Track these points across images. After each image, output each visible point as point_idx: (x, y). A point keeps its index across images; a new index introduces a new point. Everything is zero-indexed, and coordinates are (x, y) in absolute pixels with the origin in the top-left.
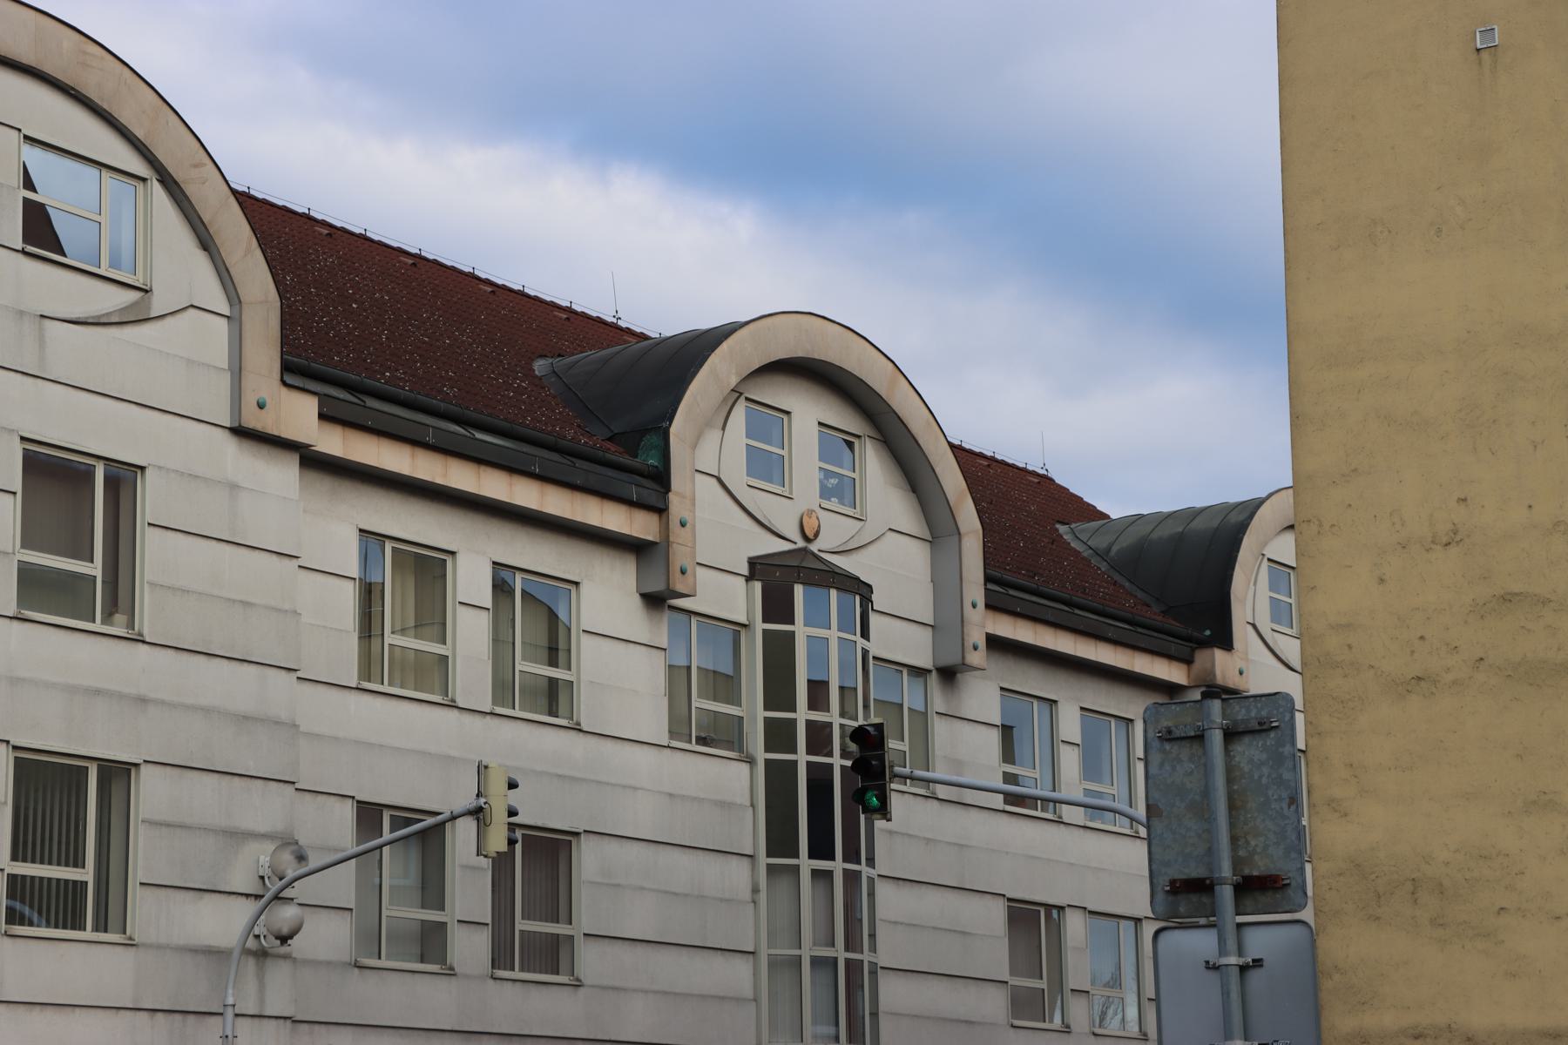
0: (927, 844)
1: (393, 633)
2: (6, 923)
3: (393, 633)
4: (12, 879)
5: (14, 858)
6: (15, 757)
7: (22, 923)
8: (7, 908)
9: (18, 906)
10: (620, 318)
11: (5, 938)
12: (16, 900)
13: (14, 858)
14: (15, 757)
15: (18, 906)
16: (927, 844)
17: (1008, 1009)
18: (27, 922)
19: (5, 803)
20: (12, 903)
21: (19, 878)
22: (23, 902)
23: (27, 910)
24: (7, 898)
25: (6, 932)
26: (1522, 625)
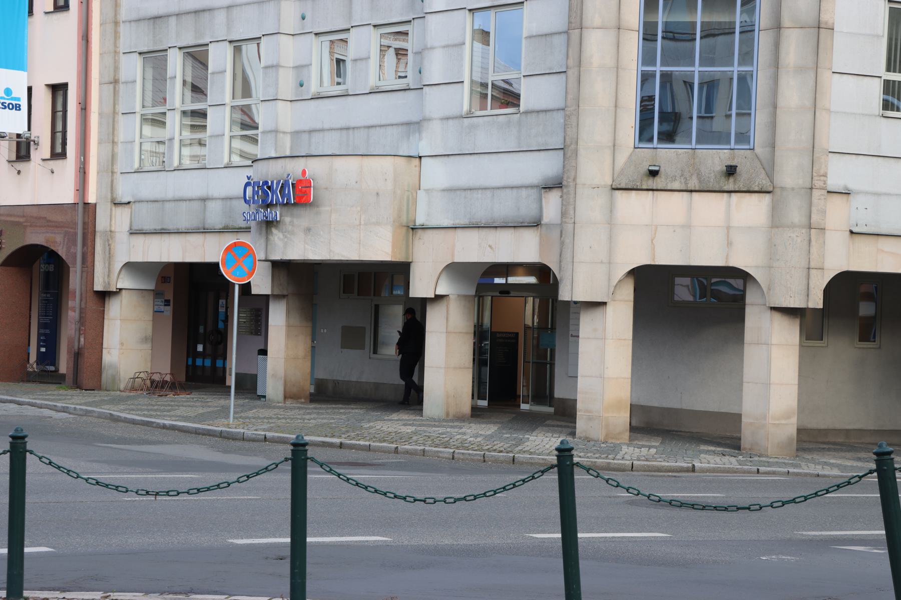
0: (602, 261)
1: (170, 278)
2: (883, 110)
3: (170, 278)
4: (887, 83)
5: (888, 69)
6: (890, 7)
7: (892, 110)
8: (883, 100)
9: (890, 98)
10: (244, 220)
11: (882, 118)
12: (889, 95)
13: (888, 69)
14: (890, 7)
15: (890, 98)
16: (602, 261)
17: (473, 382)
18: (895, 109)
19: (883, 36)
20: (886, 97)
21: (891, 82)
22: (893, 96)
23: (896, 101)
24: (884, 94)
25: (882, 115)
26: (819, 303)
